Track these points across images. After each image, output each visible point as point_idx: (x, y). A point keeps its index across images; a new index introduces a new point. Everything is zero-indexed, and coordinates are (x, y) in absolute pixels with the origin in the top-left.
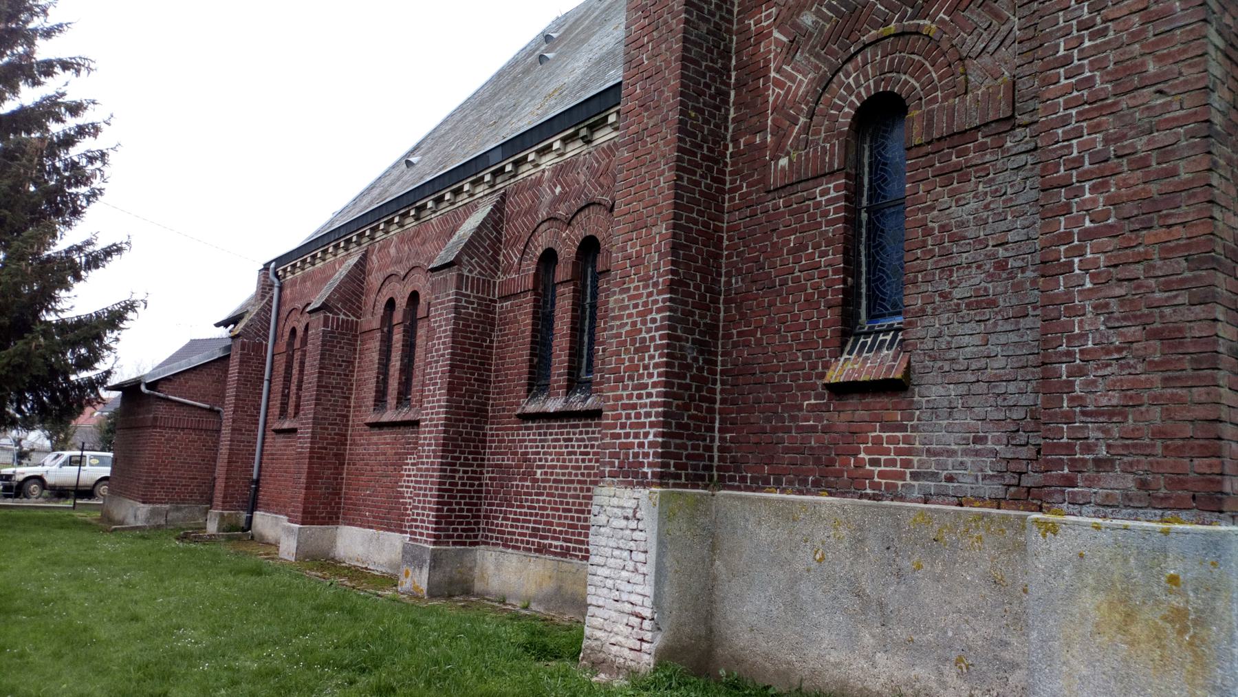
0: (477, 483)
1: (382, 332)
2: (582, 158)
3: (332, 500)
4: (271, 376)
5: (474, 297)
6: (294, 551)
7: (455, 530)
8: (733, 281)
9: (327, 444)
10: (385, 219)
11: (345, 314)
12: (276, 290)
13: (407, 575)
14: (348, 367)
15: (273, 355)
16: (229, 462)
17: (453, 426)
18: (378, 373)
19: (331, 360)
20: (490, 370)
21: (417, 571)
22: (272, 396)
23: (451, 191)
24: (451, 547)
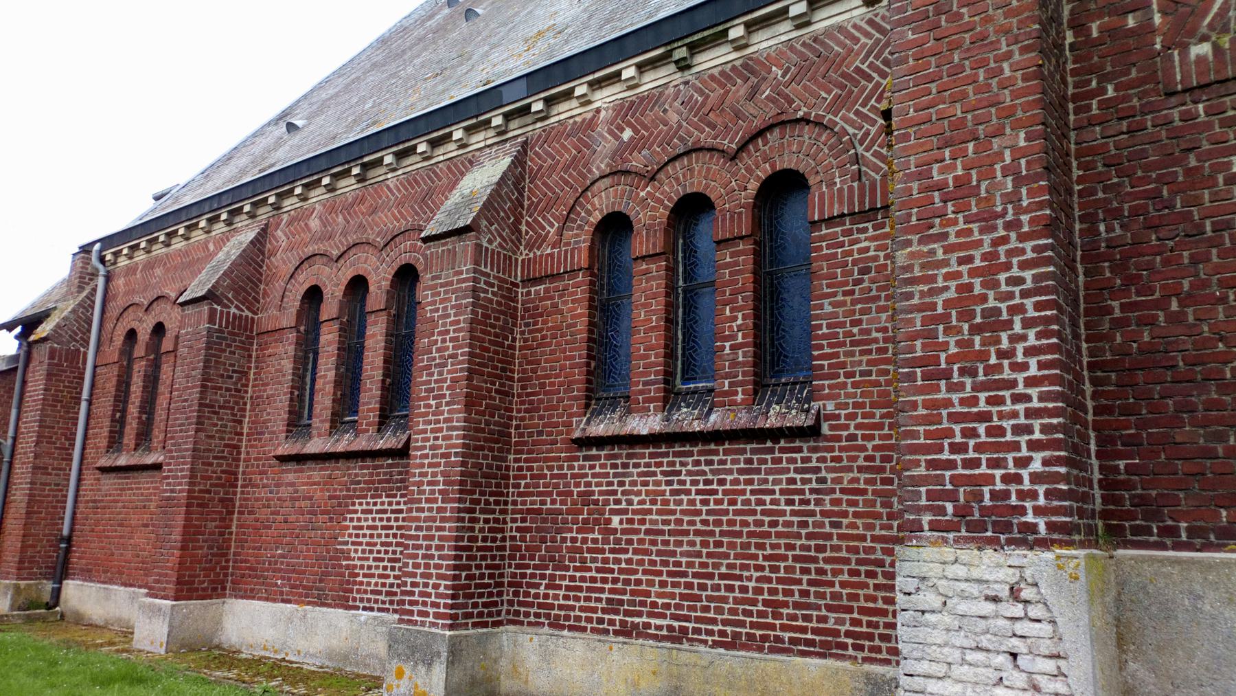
0: (499, 536)
1: (298, 331)
2: (671, 90)
3: (217, 563)
4: (91, 395)
5: (495, 277)
6: (165, 639)
7: (475, 605)
8: (1102, 228)
9: (211, 485)
10: (304, 181)
11: (237, 307)
12: (101, 281)
13: (400, 674)
14: (240, 379)
15: (95, 367)
16: (28, 513)
17: (472, 456)
18: (292, 387)
19: (217, 368)
20: (512, 379)
21: (422, 669)
22: (92, 422)
23: (428, 141)
24: (471, 631)
